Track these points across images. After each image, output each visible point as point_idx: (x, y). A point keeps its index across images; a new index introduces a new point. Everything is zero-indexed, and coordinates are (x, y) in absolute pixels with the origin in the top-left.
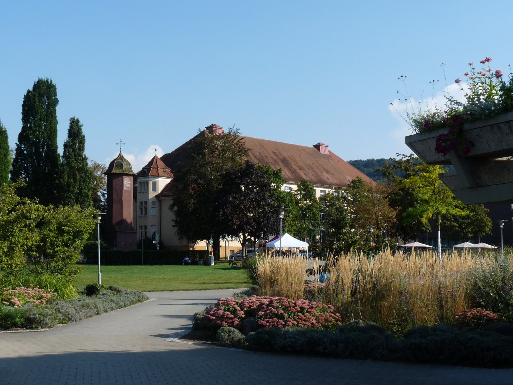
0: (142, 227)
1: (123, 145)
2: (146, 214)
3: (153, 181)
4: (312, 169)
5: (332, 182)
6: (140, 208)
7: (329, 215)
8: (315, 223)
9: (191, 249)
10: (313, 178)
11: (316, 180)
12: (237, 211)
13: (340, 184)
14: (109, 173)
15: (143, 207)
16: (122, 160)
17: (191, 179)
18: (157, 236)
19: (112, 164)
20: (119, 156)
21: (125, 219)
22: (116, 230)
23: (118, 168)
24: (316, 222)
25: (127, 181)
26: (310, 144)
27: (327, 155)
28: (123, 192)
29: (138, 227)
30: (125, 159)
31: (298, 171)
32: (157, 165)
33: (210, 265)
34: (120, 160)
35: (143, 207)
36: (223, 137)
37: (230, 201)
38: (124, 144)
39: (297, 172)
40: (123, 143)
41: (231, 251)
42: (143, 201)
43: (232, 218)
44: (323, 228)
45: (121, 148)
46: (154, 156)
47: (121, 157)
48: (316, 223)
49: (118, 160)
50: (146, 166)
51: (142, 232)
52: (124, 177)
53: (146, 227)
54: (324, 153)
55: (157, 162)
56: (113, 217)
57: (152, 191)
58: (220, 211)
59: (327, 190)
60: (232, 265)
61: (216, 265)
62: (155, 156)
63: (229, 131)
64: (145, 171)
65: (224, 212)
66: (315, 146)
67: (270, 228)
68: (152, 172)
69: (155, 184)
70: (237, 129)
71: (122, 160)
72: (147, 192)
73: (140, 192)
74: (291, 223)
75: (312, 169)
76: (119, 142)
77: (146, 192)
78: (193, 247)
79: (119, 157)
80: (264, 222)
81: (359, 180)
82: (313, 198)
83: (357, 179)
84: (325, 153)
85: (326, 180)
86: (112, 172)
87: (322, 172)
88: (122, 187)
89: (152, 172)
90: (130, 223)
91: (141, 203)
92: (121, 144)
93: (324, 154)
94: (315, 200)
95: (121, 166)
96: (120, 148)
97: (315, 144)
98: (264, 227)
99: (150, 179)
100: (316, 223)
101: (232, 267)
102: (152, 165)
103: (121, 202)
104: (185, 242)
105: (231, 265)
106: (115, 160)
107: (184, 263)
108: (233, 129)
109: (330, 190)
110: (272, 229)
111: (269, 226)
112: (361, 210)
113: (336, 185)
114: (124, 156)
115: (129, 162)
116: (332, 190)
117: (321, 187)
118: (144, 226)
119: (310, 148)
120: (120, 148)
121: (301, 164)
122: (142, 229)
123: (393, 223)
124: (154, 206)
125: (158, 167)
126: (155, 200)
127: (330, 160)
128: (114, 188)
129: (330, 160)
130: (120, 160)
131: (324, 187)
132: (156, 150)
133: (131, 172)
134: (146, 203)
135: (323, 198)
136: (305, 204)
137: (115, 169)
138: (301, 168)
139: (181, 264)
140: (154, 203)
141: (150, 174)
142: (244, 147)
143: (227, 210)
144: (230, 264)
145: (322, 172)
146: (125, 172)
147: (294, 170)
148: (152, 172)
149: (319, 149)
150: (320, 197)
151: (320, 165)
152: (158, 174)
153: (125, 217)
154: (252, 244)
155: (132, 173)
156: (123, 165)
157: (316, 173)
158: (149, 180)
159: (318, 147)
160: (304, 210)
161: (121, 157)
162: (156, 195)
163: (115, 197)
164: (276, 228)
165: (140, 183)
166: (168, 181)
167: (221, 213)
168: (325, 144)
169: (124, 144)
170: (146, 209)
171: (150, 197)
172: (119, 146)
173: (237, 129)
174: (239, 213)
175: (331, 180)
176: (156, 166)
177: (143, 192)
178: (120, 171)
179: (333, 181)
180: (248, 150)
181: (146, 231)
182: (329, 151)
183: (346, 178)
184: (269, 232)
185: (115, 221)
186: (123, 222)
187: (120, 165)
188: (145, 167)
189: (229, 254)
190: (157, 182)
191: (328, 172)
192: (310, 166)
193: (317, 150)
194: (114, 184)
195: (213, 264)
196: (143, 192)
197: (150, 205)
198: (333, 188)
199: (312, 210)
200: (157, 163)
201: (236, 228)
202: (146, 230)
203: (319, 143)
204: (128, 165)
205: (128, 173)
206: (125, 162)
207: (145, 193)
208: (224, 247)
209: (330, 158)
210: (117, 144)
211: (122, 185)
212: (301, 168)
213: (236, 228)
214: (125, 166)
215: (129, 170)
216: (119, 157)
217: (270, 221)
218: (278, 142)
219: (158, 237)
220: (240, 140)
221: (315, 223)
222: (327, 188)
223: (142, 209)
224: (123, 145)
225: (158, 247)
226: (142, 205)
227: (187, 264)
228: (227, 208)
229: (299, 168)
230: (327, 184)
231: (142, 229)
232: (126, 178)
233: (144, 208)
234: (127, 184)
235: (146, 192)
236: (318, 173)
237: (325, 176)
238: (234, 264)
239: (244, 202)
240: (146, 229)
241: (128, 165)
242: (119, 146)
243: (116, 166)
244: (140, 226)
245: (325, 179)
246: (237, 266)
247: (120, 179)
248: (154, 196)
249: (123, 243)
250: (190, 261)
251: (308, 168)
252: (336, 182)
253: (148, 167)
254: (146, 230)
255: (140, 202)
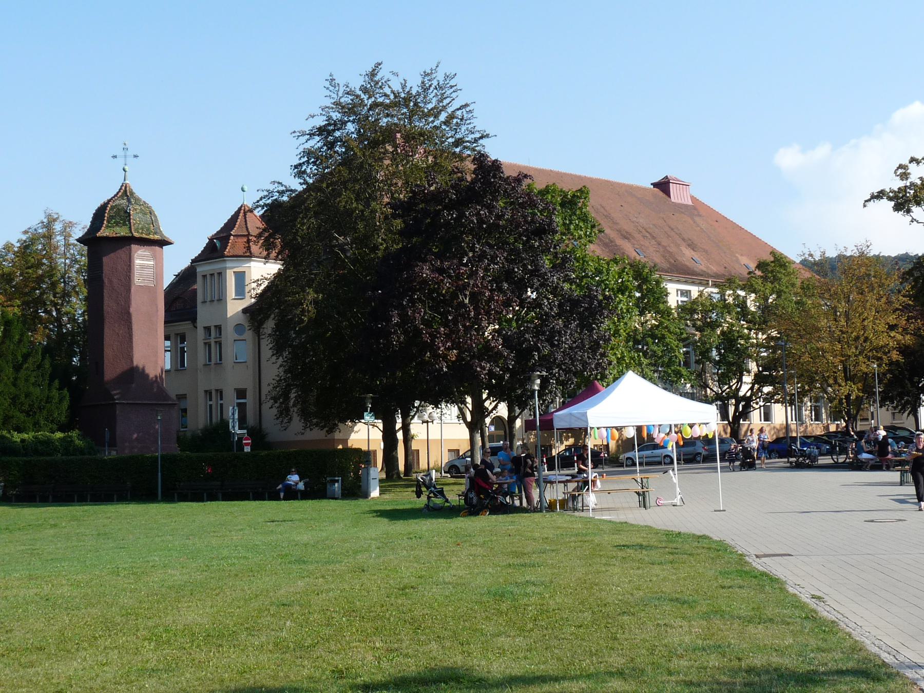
0: (210, 393)
1: (131, 160)
2: (221, 359)
3: (236, 270)
4: (653, 238)
5: (705, 269)
6: (205, 343)
7: (704, 350)
8: (670, 372)
9: (340, 447)
10: (658, 259)
11: (665, 265)
12: (449, 313)
13: (727, 274)
14: (90, 240)
15: (212, 341)
16: (129, 201)
17: (308, 228)
18: (233, 414)
19: (99, 216)
20: (121, 189)
21: (141, 367)
23: (117, 224)
24: (673, 368)
25: (143, 260)
26: (646, 180)
27: (686, 206)
29: (201, 394)
30: (138, 200)
31: (620, 242)
33: (366, 495)
34: (122, 201)
35: (212, 341)
36: (407, 100)
37: (425, 282)
38: (136, 156)
39: (616, 246)
40: (130, 153)
41: (449, 450)
42: (212, 324)
43: (433, 337)
44: (688, 386)
45: (127, 168)
46: (240, 206)
47: (125, 193)
48: (673, 371)
49: (117, 202)
50: (218, 232)
51: (211, 406)
52: (134, 247)
53: (221, 392)
54: (680, 201)
55: (246, 221)
56: (106, 361)
58: (392, 316)
59: (695, 291)
60: (429, 498)
61: (387, 496)
62: (242, 206)
63: (423, 82)
64: (215, 244)
65: (404, 317)
66: (655, 185)
67: (559, 366)
68: (233, 247)
69: (240, 277)
70: (446, 77)
71: (129, 201)
72: (220, 299)
73: (204, 302)
74: (623, 357)
75: (653, 238)
76: (120, 153)
78: (345, 441)
79: (120, 194)
80: (538, 350)
81: (778, 260)
82: (661, 306)
83: (772, 259)
84: (683, 202)
85: (690, 264)
87: (678, 246)
88: (130, 278)
89: (235, 245)
90: (156, 377)
91: (207, 329)
92: (125, 156)
93: (679, 204)
94: (667, 312)
95: (124, 217)
96: (124, 170)
97: (656, 180)
98: (539, 365)
99: (228, 265)
100: (673, 371)
101: (427, 506)
103: (126, 318)
104: (316, 434)
105: (424, 498)
106: (109, 201)
107: (282, 495)
108: (434, 76)
109: (701, 288)
110: (567, 372)
111: (555, 359)
112: (799, 331)
113: (717, 276)
115: (149, 208)
116: (706, 290)
117: (678, 282)
118: (217, 390)
119: (645, 189)
120: (124, 170)
121: (627, 226)
122: (211, 400)
123: (891, 363)
126: (243, 320)
127: (697, 219)
128: (106, 281)
129: (697, 219)
131: (686, 282)
133: (155, 233)
134: (219, 328)
135: (688, 309)
136: (642, 324)
137: (107, 227)
138: (626, 236)
139: (275, 497)
140: (239, 328)
141: (229, 252)
142: (472, 126)
143: (414, 312)
144: (419, 494)
145: (678, 246)
146: (136, 235)
147: (609, 239)
149: (667, 193)
150: (678, 305)
151: (672, 229)
152: (250, 252)
153: (139, 359)
154: (505, 432)
155: (157, 237)
156: (129, 215)
157: (664, 247)
158: (226, 268)
159: (663, 186)
160: (639, 338)
161: (125, 193)
162: (245, 306)
163: (109, 305)
164: (580, 367)
165: (204, 276)
166: (273, 268)
167: (396, 320)
168: (679, 178)
169: (136, 156)
170: (220, 344)
171: (229, 314)
172: (120, 162)
173: (446, 77)
174: (455, 321)
175: (702, 265)
176: (245, 229)
177: (212, 301)
178: (122, 232)
179: (708, 267)
180: (481, 138)
181: (221, 405)
182: (692, 198)
183: (737, 261)
184: (557, 380)
185: (111, 371)
186: (134, 375)
189: (445, 461)
191: (692, 246)
192: (649, 230)
193: (661, 194)
194: (106, 269)
195: (375, 493)
196: (212, 301)
197: (229, 333)
198: (708, 284)
199: (663, 337)
200: (246, 224)
201: (445, 369)
202: (222, 402)
203: (667, 177)
204: (145, 214)
205: (144, 236)
206: (138, 207)
208: (421, 440)
209: (696, 213)
211: (130, 272)
212: (626, 236)
213: (445, 369)
214: (136, 217)
215: (148, 229)
216: (120, 194)
217: (558, 346)
218: (565, 174)
219: (236, 416)
220: (458, 109)
221: (670, 372)
222: (693, 283)
224: (131, 160)
225: (247, 444)
226: (210, 335)
227: (291, 494)
228: (413, 306)
229: (622, 235)
230: (694, 273)
231: (211, 400)
232: (139, 252)
234: (143, 267)
236: (668, 248)
237: (687, 255)
238: (436, 496)
239: (472, 282)
240: (221, 399)
241: (145, 214)
242: (120, 162)
243: (111, 218)
245: (687, 264)
246: (447, 501)
247: (121, 253)
248: (240, 308)
249: (135, 436)
250: (301, 486)
251: (644, 237)
252: (714, 269)
253: (225, 235)
254: (222, 402)
255: (204, 328)
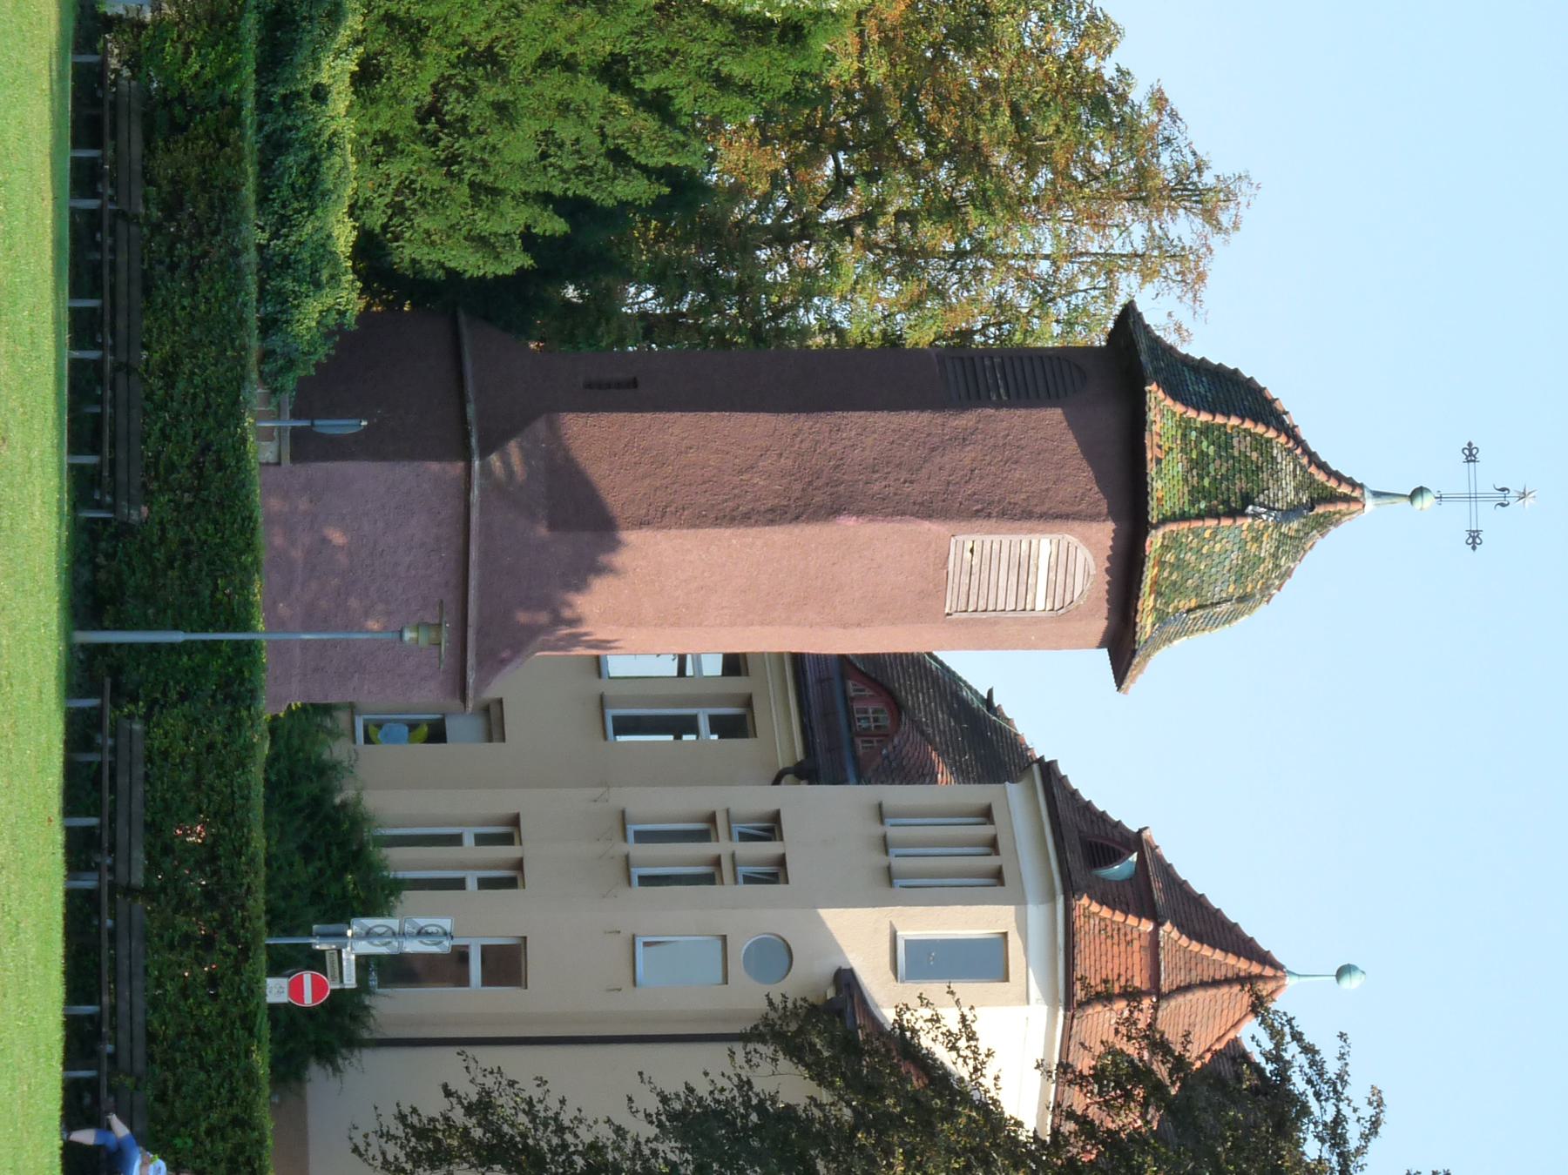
0: (507, 839)
1: (1458, 518)
2: (646, 881)
6: (712, 819)
15: (721, 847)
16: (1293, 511)
18: (421, 933)
20: (1340, 478)
22: (485, 453)
23: (1198, 464)
28: (926, 525)
29: (502, 803)
30: (1296, 546)
32: (1188, 988)
35: (721, 847)
38: (1474, 539)
40: (1488, 517)
42: (793, 845)
45: (1427, 501)
46: (1278, 956)
49: (1286, 465)
51: (455, 840)
52: (1104, 533)
56: (639, 419)
57: (905, 934)
62: (1277, 966)
68: (1108, 931)
71: (1293, 511)
73: (881, 814)
76: (1488, 475)
77: (890, 876)
79: (1321, 477)
86: (1154, 393)
91: (771, 828)
92: (1473, 497)
96: (1419, 492)
99: (1036, 913)
102: (1182, 928)
106: (1291, 433)
107: (86, 1137)
114: (1334, 532)
115: (1266, 592)
118: (519, 865)
120: (1419, 492)
124: (736, 968)
125: (1161, 996)
130: (1287, 491)
132: (1343, 972)
133: (1161, 618)
134: (776, 873)
137: (1185, 426)
140: (779, 954)
141: (1088, 916)
146: (1154, 541)
148: (1104, 924)
155: (1146, 622)
158: (1019, 900)
165: (987, 815)
169: (1474, 539)
171: (825, 913)
172: (1448, 474)
176: (1181, 979)
177: (885, 845)
181: (459, 884)
187: (1240, 484)
188: (1159, 859)
190: (998, 987)
196: (885, 845)
200: (1203, 985)
202: (472, 884)
204: (1240, 577)
205: (1150, 573)
206: (1268, 546)
207: (880, 860)
210: (1471, 455)
211: (1003, 514)
216: (1321, 477)
223: (703, 836)
224: (1458, 518)
225: (296, 989)
226: (745, 837)
231: (482, 840)
233: (717, 862)
234: (1024, 567)
235: (890, 876)
240: (485, 884)
242: (1448, 474)
243: (1224, 442)
244: (515, 821)
247: (1081, 480)
249: (337, 537)
253: (1158, 895)
254: (472, 884)
